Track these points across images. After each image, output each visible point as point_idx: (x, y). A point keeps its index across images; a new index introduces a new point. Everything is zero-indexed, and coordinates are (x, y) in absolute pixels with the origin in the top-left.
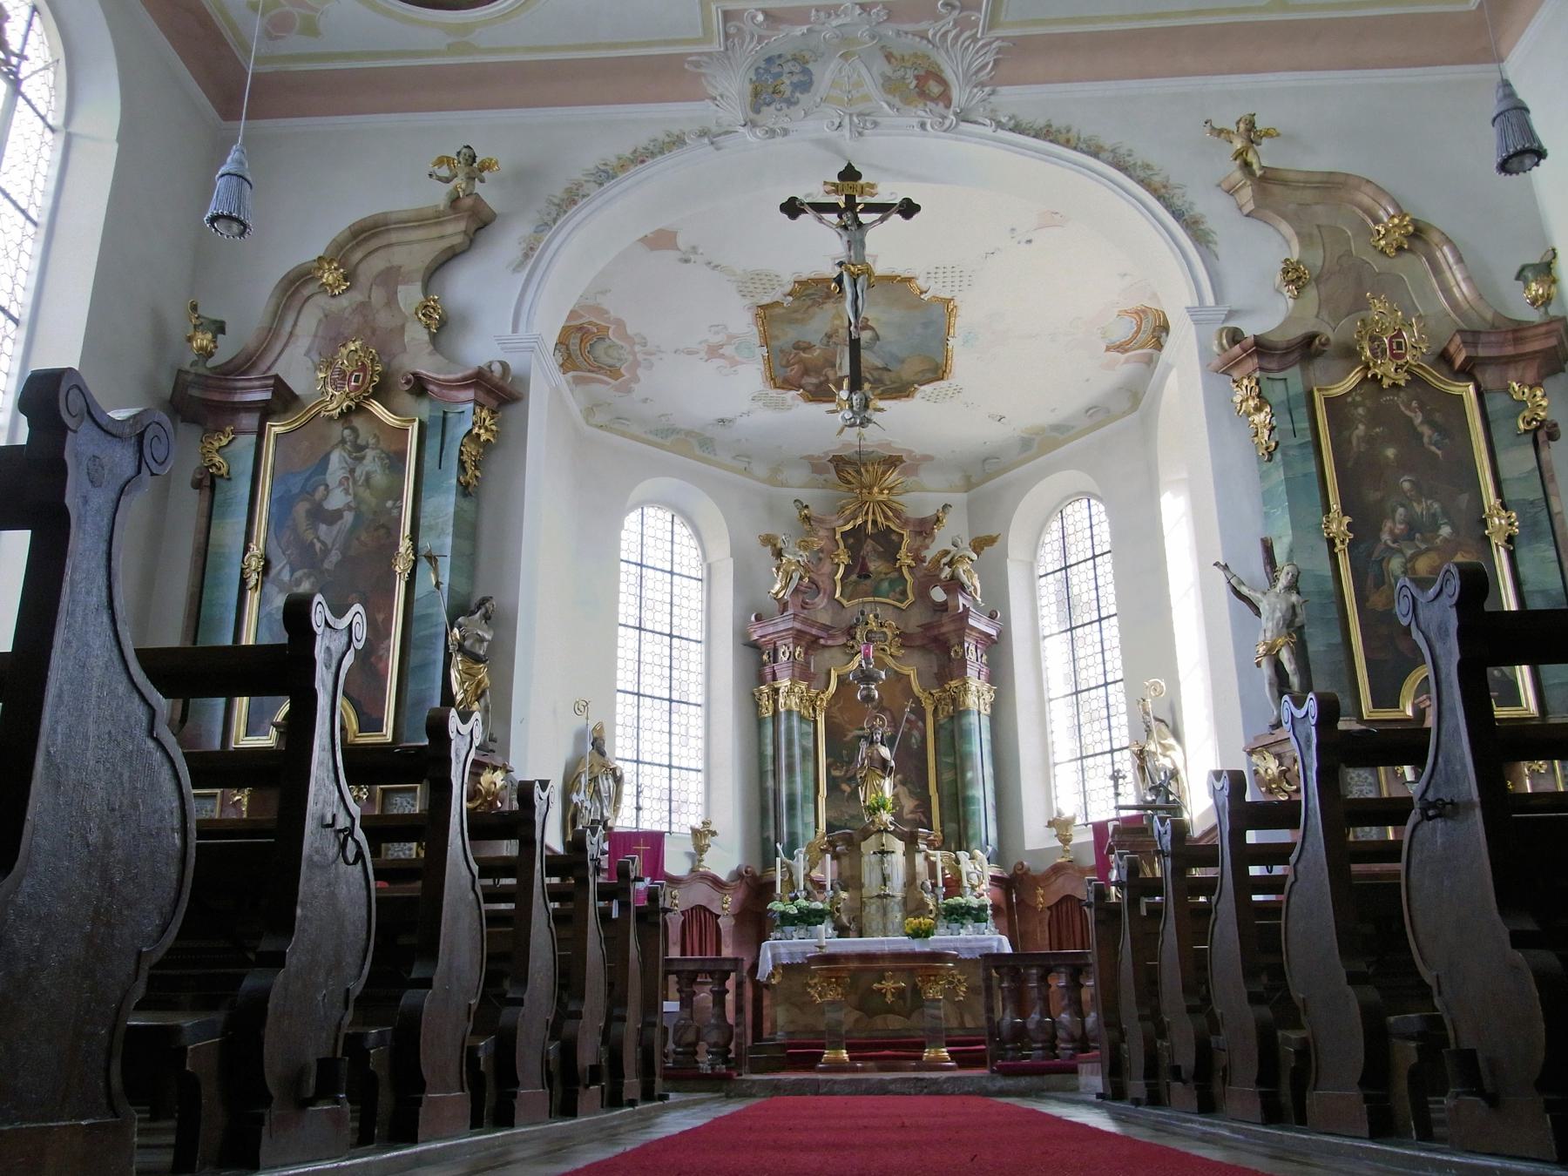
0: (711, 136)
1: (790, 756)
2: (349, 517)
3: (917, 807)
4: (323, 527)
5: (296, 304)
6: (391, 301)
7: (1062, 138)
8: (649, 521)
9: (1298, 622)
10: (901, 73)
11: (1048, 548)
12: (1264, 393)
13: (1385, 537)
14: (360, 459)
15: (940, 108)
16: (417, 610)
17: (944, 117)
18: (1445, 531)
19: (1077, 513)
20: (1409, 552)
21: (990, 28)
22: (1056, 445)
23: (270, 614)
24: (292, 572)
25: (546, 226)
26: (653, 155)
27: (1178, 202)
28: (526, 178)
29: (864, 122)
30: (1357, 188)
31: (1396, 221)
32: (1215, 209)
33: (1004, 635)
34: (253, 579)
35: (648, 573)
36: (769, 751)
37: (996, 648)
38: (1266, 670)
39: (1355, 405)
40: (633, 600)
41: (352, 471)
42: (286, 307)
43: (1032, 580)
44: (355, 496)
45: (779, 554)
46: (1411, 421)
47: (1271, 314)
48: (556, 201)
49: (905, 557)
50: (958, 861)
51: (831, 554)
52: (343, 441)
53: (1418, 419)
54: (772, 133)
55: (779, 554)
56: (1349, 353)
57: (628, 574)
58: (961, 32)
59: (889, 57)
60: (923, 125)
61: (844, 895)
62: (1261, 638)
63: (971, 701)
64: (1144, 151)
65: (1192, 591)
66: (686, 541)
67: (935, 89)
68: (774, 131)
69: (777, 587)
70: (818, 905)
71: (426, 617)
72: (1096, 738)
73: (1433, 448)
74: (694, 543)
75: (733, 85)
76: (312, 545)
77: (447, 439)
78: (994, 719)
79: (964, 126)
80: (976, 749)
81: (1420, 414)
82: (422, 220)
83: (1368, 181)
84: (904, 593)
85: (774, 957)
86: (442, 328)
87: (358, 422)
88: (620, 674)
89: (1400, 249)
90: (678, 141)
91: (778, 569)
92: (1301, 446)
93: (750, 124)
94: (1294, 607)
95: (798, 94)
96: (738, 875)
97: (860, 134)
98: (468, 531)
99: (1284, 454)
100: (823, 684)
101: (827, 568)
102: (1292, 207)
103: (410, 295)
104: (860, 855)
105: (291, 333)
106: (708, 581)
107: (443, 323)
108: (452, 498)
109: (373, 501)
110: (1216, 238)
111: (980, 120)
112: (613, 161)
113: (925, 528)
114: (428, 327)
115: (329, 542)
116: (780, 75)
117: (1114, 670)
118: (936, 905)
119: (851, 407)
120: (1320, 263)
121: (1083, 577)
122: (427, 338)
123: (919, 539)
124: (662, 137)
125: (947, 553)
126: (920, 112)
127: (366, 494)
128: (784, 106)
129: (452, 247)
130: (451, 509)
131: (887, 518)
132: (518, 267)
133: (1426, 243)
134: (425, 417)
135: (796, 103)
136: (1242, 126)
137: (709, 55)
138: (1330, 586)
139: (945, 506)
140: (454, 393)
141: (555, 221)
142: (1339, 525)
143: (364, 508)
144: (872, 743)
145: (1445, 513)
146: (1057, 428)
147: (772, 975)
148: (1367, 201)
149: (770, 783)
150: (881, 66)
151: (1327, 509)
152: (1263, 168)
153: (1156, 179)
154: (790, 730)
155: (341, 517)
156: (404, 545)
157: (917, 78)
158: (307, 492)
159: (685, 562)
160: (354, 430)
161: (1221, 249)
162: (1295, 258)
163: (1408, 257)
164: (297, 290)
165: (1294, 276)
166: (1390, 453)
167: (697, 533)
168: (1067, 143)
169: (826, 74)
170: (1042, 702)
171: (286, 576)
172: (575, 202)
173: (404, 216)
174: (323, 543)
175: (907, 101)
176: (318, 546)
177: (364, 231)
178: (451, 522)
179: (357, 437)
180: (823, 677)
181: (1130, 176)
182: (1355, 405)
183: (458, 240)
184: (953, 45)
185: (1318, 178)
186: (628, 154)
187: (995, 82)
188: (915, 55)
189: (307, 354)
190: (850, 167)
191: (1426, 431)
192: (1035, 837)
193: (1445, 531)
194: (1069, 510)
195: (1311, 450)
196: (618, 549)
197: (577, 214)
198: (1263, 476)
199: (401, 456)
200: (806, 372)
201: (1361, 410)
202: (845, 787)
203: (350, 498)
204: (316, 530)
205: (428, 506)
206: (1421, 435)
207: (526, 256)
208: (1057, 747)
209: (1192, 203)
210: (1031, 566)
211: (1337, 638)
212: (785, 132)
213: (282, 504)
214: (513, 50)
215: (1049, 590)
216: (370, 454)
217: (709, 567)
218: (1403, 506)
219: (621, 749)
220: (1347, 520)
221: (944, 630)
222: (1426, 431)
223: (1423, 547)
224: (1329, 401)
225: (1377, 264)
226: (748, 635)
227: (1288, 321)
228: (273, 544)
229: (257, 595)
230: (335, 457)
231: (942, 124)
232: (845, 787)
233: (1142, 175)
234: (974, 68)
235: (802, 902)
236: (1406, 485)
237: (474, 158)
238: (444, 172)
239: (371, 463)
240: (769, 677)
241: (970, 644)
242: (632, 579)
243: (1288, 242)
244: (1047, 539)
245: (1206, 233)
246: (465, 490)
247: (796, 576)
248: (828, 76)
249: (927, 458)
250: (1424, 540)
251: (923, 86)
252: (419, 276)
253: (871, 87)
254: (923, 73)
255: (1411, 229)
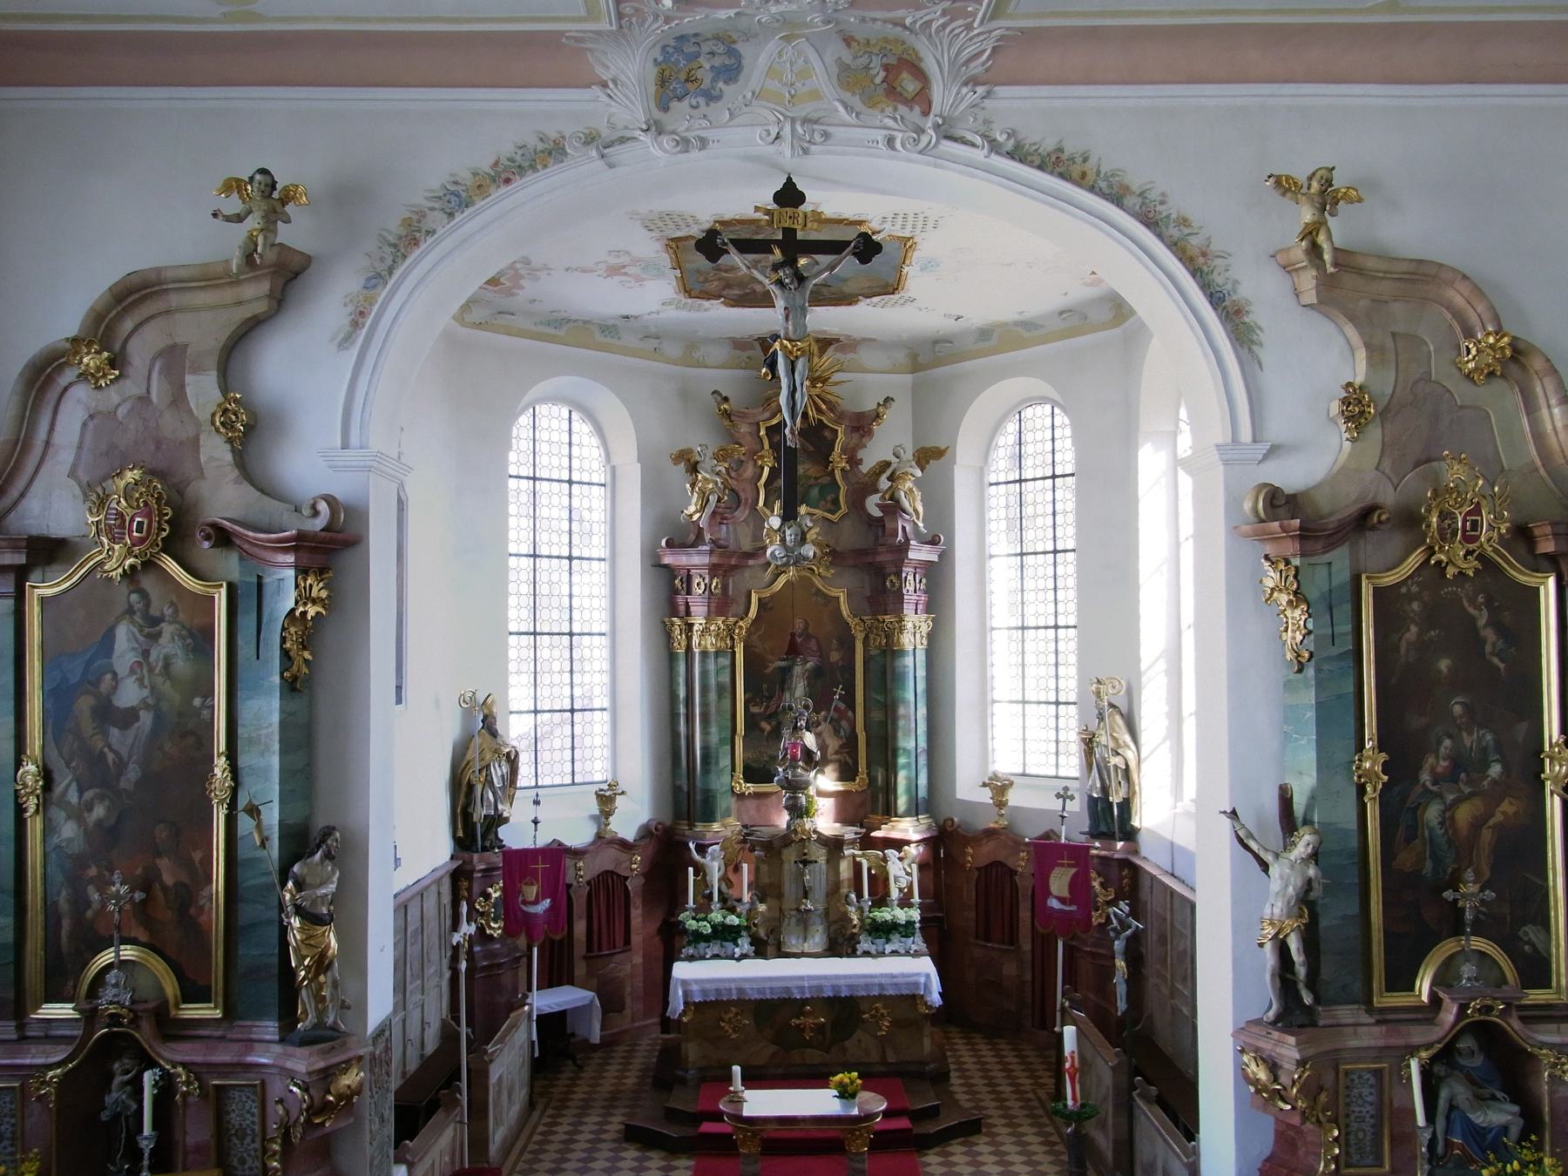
0: (602, 143)
1: (704, 704)
2: (146, 718)
3: (842, 747)
4: (115, 732)
5: (52, 396)
6: (178, 398)
7: (1076, 171)
8: (543, 423)
9: (1313, 895)
10: (863, 61)
11: (1001, 452)
12: (1302, 590)
13: (1425, 777)
14: (155, 637)
15: (915, 115)
16: (243, 852)
17: (920, 131)
18: (1495, 770)
19: (1038, 415)
20: (1450, 797)
21: (993, 18)
22: (1022, 344)
23: (58, 847)
24: (81, 792)
25: (377, 279)
26: (521, 171)
27: (1219, 279)
28: (348, 197)
29: (813, 131)
30: (1451, 284)
31: (1491, 340)
32: (1266, 291)
33: (947, 557)
34: (32, 804)
35: (543, 487)
36: (682, 693)
37: (938, 578)
38: (1269, 957)
39: (1410, 598)
40: (526, 523)
41: (146, 654)
42: (36, 408)
43: (982, 485)
44: (153, 688)
45: (694, 469)
46: (1473, 620)
47: (1320, 457)
48: (391, 239)
49: (838, 460)
50: (885, 859)
51: (753, 454)
52: (130, 611)
53: (1482, 618)
54: (684, 144)
55: (694, 469)
56: (1409, 520)
57: (518, 490)
58: (952, 20)
59: (848, 41)
60: (890, 142)
61: (762, 908)
62: (1267, 911)
63: (907, 640)
64: (1185, 198)
65: (1165, 568)
66: (586, 440)
67: (910, 85)
68: (686, 141)
69: (692, 509)
70: (733, 920)
71: (252, 862)
72: (1040, 611)
73: (1496, 660)
74: (595, 441)
75: (632, 68)
76: (102, 755)
77: (265, 619)
78: (930, 653)
79: (947, 146)
80: (910, 696)
81: (1485, 613)
82: (210, 278)
83: (1465, 277)
84: (836, 502)
85: (685, 993)
86: (250, 431)
87: (148, 582)
88: (512, 535)
89: (1491, 374)
90: (553, 151)
91: (693, 486)
92: (1341, 657)
93: (656, 128)
94: (1310, 881)
95: (721, 85)
96: (646, 832)
97: (806, 151)
98: (301, 740)
99: (1318, 670)
100: (742, 609)
101: (749, 471)
102: (1363, 303)
103: (203, 391)
104: (782, 863)
105: (48, 443)
106: (612, 486)
107: (250, 428)
108: (276, 703)
109: (177, 697)
110: (1263, 337)
111: (969, 136)
112: (465, 176)
113: (863, 425)
114: (230, 441)
115: (124, 753)
116: (697, 55)
117: (1066, 614)
118: (861, 920)
119: (783, 540)
120: (1390, 391)
121: (1041, 571)
122: (229, 457)
123: (856, 436)
124: (533, 142)
125: (888, 464)
126: (886, 119)
127: (166, 687)
128: (702, 101)
129: (255, 317)
130: (275, 718)
131: (819, 410)
132: (346, 341)
133: (1523, 367)
134: (235, 574)
135: (718, 98)
136: (1315, 184)
137: (599, 33)
138: (1354, 843)
139: (888, 400)
140: (268, 555)
141: (390, 271)
142: (1372, 761)
143: (165, 706)
144: (796, 728)
145: (1499, 746)
146: (1027, 325)
147: (684, 1012)
148: (1459, 301)
149: (682, 728)
150: (836, 50)
151: (1360, 746)
152: (1336, 250)
153: (1194, 241)
154: (704, 674)
155: (137, 718)
156: (220, 764)
157: (886, 68)
158: (91, 681)
159: (586, 465)
160: (144, 595)
161: (1266, 355)
162: (1359, 380)
163: (1499, 385)
164: (50, 380)
165: (1355, 409)
166: (1444, 665)
167: (599, 430)
168: (1080, 181)
169: (760, 59)
170: (983, 630)
171: (73, 797)
172: (416, 242)
173: (184, 273)
174: (115, 752)
175: (871, 103)
176: (110, 757)
177: (130, 293)
178: (277, 738)
179: (148, 605)
180: (743, 600)
181: (1160, 236)
182: (1410, 598)
183: (260, 307)
184: (937, 31)
185: (1404, 267)
186: (485, 165)
187: (986, 81)
188: (886, 40)
189: (72, 474)
190: (790, 184)
191: (1489, 635)
192: (968, 787)
193: (1495, 770)
194: (1028, 413)
195: (1350, 662)
196: (505, 541)
197: (422, 261)
198: (1288, 686)
199: (208, 633)
200: (728, 286)
201: (1415, 606)
202: (766, 726)
203: (146, 693)
204: (105, 734)
205: (249, 709)
206: (1483, 642)
207: (356, 325)
208: (996, 683)
209: (1236, 282)
210: (981, 472)
211: (1354, 909)
212: (703, 143)
213: (58, 697)
214: (316, 19)
215: (999, 500)
216: (167, 629)
217: (613, 469)
218: (1450, 736)
219: (516, 730)
220: (1383, 757)
221: (879, 558)
222: (1489, 635)
223: (1467, 790)
224: (1379, 593)
225: (1463, 392)
226: (659, 557)
227: (1339, 475)
228: (54, 754)
229: (39, 819)
230: (123, 633)
231: (916, 141)
232: (766, 726)
233: (1174, 232)
234: (966, 54)
235: (716, 916)
236: (1457, 709)
237: (273, 186)
238: (233, 205)
239: (169, 644)
240: (682, 608)
241: (907, 571)
242: (524, 498)
243: (1352, 350)
244: (1001, 441)
245: (1250, 329)
246: (292, 686)
247: (713, 499)
248: (763, 60)
249: (864, 340)
250: (1469, 783)
251: (892, 80)
252: (212, 361)
253: (821, 78)
254: (892, 61)
255: (1508, 353)
